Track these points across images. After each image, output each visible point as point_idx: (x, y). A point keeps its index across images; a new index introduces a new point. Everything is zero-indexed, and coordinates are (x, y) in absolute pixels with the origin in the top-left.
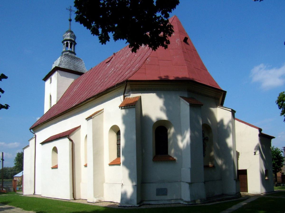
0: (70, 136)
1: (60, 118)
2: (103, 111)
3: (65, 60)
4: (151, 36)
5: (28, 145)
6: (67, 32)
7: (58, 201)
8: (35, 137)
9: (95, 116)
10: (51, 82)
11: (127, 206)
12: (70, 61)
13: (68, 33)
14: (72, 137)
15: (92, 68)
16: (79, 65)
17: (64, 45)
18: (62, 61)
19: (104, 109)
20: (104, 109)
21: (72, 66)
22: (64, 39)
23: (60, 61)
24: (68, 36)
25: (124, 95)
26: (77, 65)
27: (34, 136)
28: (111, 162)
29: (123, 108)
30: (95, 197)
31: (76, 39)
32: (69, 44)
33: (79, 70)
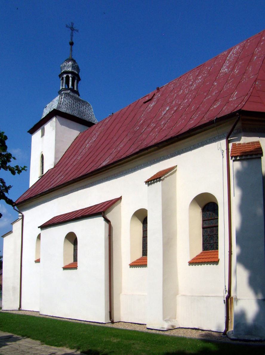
0: (106, 214)
1: (76, 185)
2: (176, 170)
3: (67, 102)
4: (207, 68)
5: (11, 231)
6: (68, 60)
7: (61, 321)
8: (23, 219)
9: (165, 177)
10: (43, 135)
11: (252, 339)
12: (74, 104)
13: (69, 62)
14: (109, 216)
15: (113, 114)
16: (86, 111)
17: (61, 80)
18: (62, 102)
19: (177, 166)
20: (177, 166)
21: (76, 111)
22: (62, 72)
23: (59, 103)
24: (68, 67)
25: (228, 138)
26: (83, 111)
27: (20, 216)
28: (192, 258)
29: (238, 158)
30: (165, 319)
31: (79, 72)
32: (70, 78)
33: (85, 118)
